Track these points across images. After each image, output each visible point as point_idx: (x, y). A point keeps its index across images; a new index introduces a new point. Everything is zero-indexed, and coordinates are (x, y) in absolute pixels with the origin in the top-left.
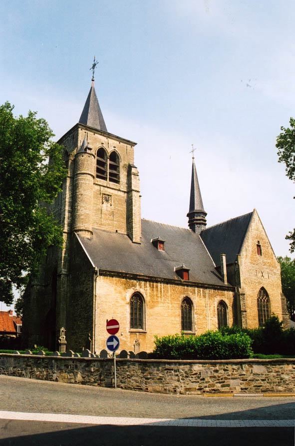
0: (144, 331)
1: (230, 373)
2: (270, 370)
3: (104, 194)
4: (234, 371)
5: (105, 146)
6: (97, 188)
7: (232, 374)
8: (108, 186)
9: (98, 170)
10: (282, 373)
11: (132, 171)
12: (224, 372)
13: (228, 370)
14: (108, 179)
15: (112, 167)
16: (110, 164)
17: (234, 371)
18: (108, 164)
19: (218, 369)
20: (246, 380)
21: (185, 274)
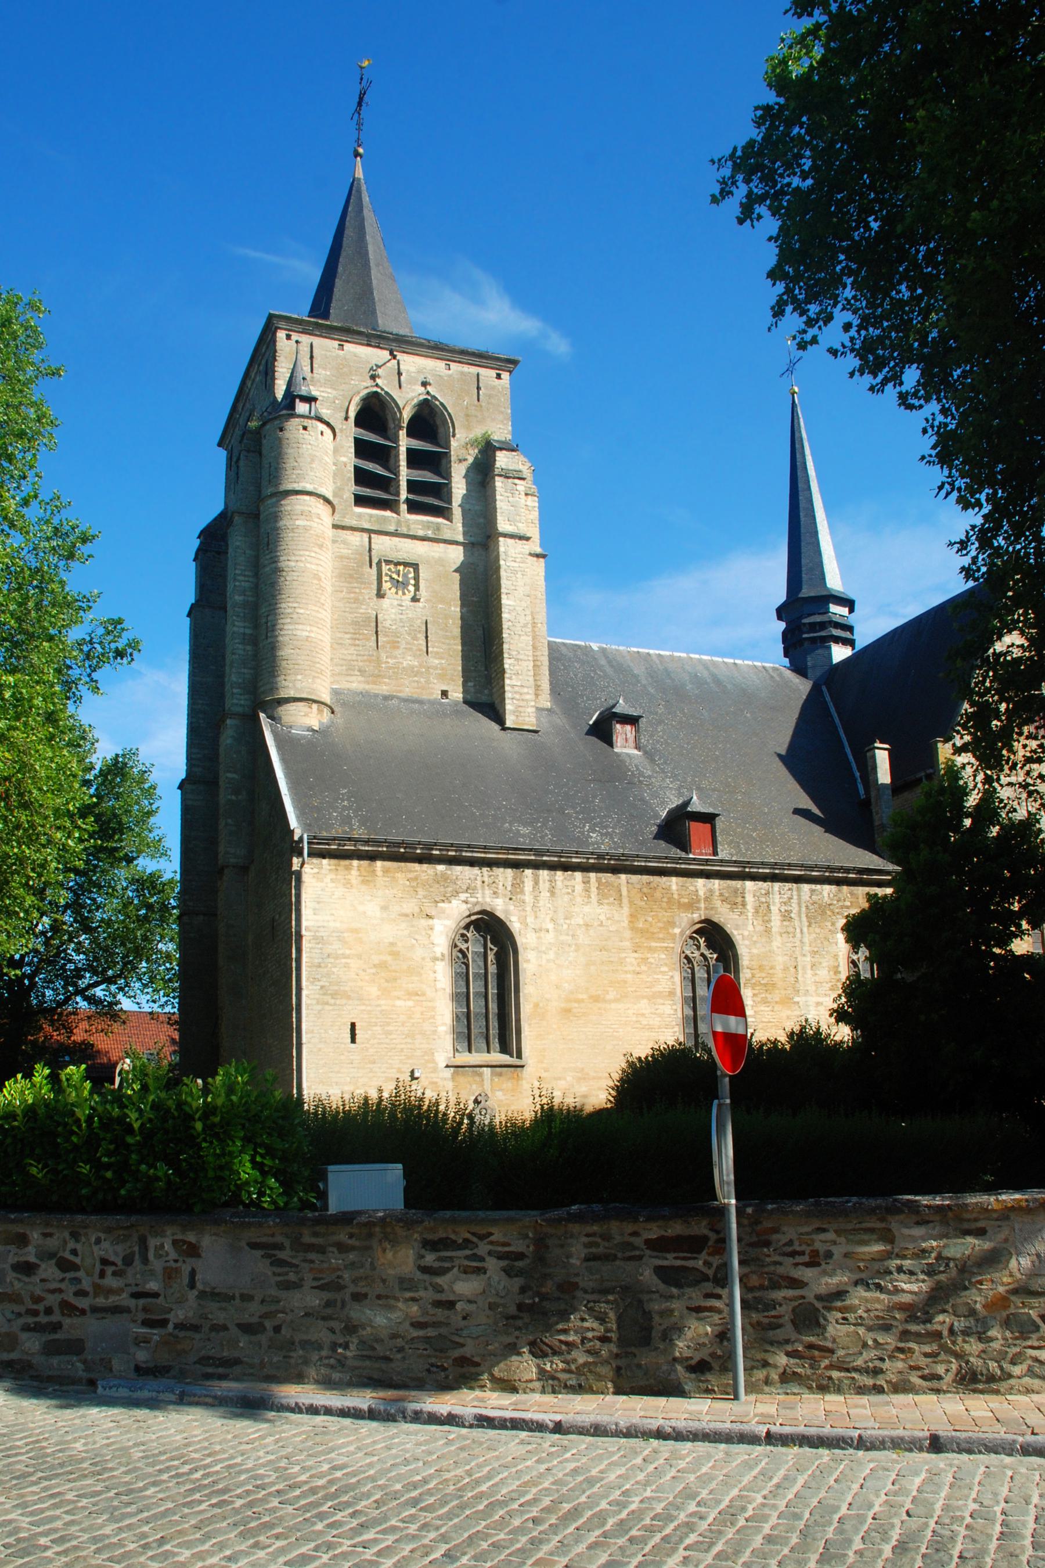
0: (518, 1062)
1: (86, 1284)
2: (292, 1277)
3: (388, 562)
4: (109, 1270)
5: (386, 384)
6: (358, 540)
7: (98, 1290)
8: (404, 530)
9: (361, 477)
10: (358, 1297)
11: (498, 464)
12: (58, 1274)
13: (75, 1267)
14: (404, 507)
15: (415, 459)
16: (409, 451)
17: (109, 1270)
18: (403, 450)
19: (32, 1259)
20: (163, 1323)
21: (697, 830)
